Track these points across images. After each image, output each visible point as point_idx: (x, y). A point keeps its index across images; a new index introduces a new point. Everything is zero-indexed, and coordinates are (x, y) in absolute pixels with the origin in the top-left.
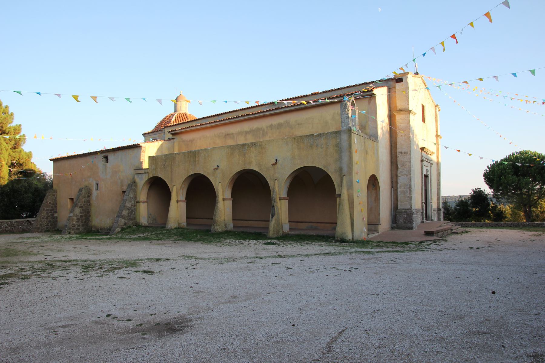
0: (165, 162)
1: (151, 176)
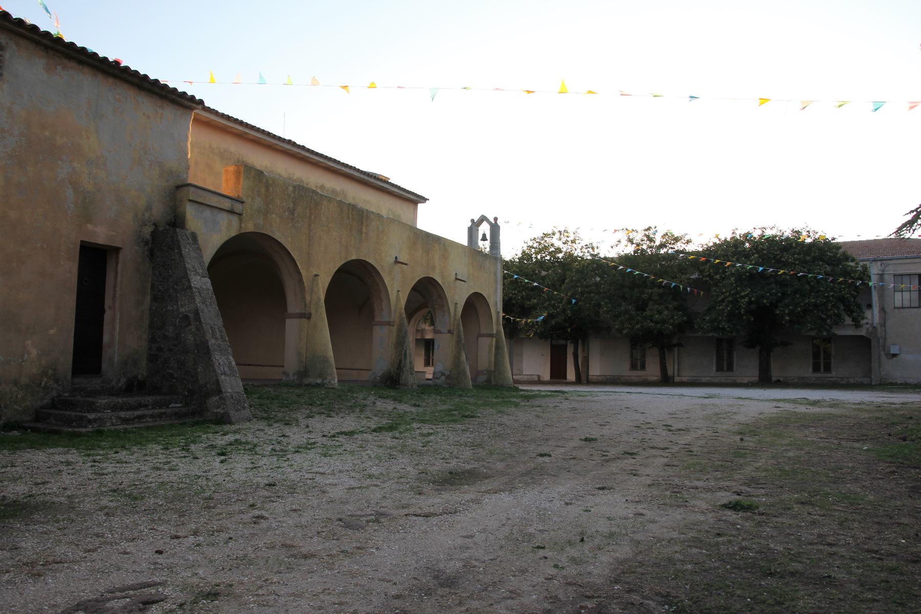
0: (294, 203)
1: (250, 227)
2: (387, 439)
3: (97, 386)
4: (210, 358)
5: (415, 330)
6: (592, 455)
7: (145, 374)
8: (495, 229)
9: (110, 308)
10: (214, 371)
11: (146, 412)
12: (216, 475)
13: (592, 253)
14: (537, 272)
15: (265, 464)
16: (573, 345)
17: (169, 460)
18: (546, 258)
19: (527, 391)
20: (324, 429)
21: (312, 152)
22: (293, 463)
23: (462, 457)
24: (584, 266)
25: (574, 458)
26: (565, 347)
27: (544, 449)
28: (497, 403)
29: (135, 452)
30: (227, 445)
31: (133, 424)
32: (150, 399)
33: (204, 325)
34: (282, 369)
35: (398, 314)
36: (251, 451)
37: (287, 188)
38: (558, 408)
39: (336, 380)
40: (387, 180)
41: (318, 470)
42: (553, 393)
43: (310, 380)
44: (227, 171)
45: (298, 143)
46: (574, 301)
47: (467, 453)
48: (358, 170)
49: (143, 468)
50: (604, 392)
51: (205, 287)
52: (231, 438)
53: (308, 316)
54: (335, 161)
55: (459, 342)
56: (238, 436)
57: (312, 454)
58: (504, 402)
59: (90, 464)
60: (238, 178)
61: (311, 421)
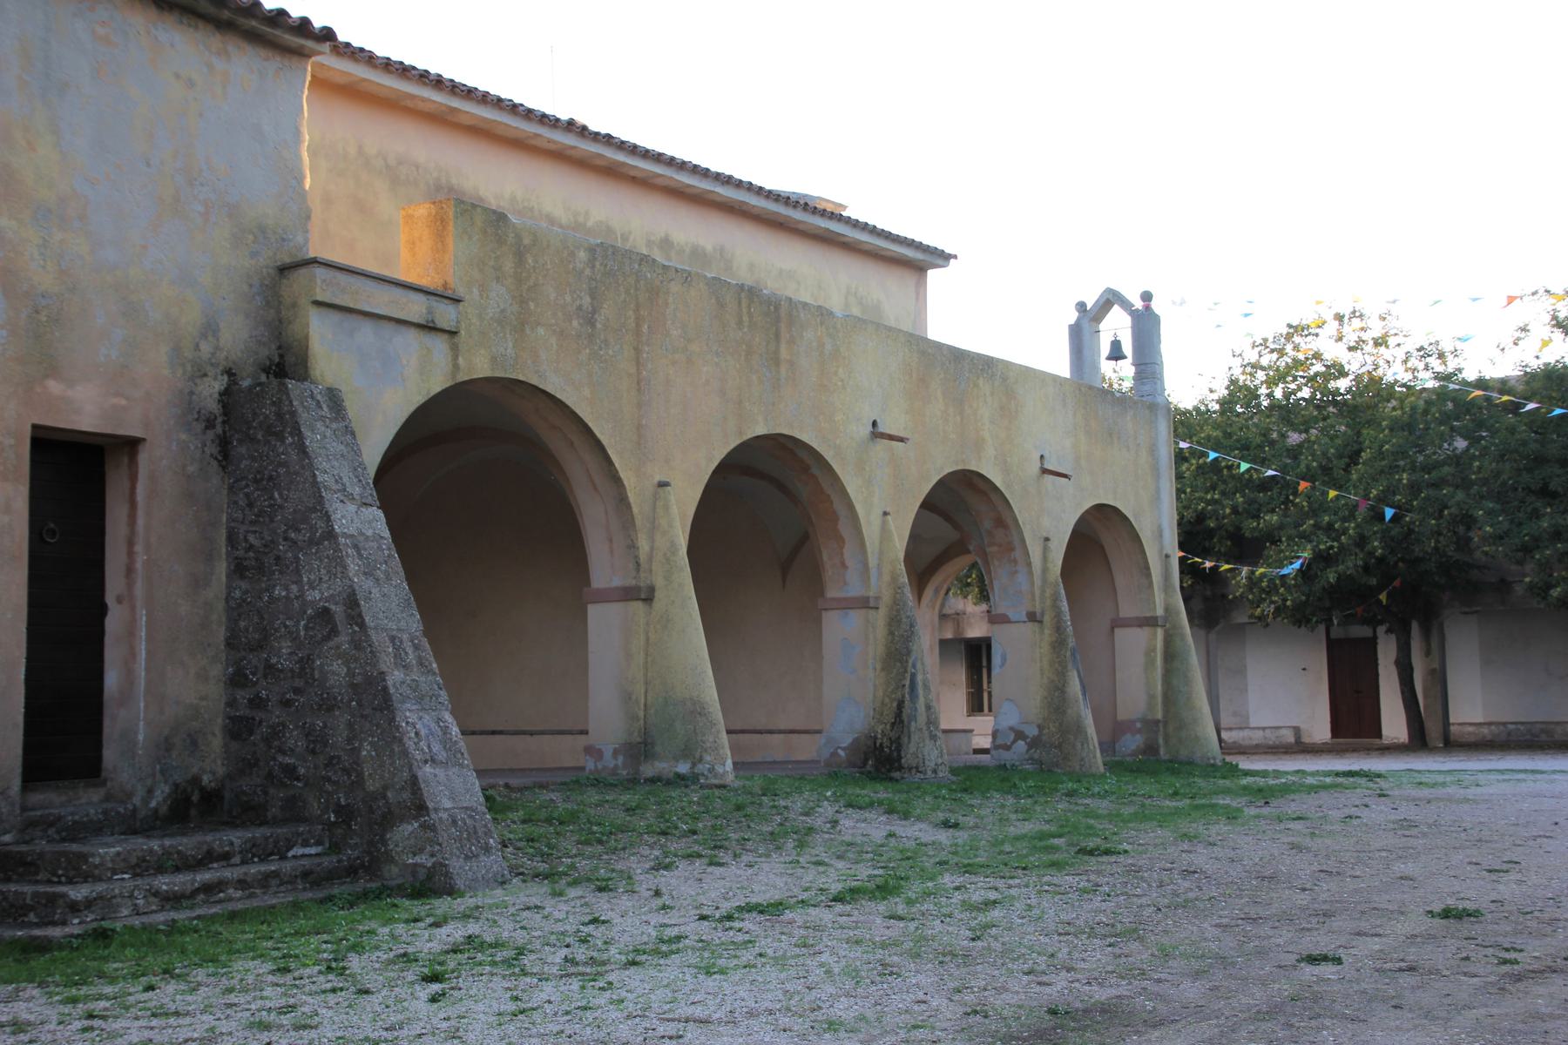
0: (593, 294)
1: (479, 366)
2: (873, 918)
3: (92, 811)
4: (393, 719)
5: (936, 619)
6: (1467, 958)
7: (221, 771)
8: (1146, 324)
9: (119, 600)
10: (405, 753)
11: (228, 874)
12: (420, 1036)
13: (1440, 369)
14: (1275, 435)
15: (550, 1002)
16: (1393, 637)
17: (292, 1001)
18: (1299, 395)
19: (1264, 774)
20: (702, 899)
21: (634, 150)
22: (624, 994)
23: (1082, 965)
24: (1413, 408)
25: (1411, 969)
26: (1372, 643)
27: (1321, 942)
28: (1177, 812)
29: (199, 984)
30: (447, 952)
31: (192, 908)
32: (236, 838)
33: (372, 633)
34: (582, 741)
35: (886, 578)
36: (511, 966)
37: (572, 254)
38: (1355, 822)
39: (729, 763)
40: (836, 212)
41: (691, 1011)
42: (1340, 780)
43: (660, 767)
44: (409, 218)
45: (593, 127)
46: (1389, 513)
47: (1097, 956)
48: (760, 191)
49: (224, 1027)
50: (1501, 772)
51: (370, 533)
52: (455, 932)
53: (648, 596)
54: (695, 170)
55: (1059, 644)
56: (473, 928)
57: (672, 969)
58: (1197, 807)
59: (78, 1025)
60: (440, 236)
61: (665, 879)
